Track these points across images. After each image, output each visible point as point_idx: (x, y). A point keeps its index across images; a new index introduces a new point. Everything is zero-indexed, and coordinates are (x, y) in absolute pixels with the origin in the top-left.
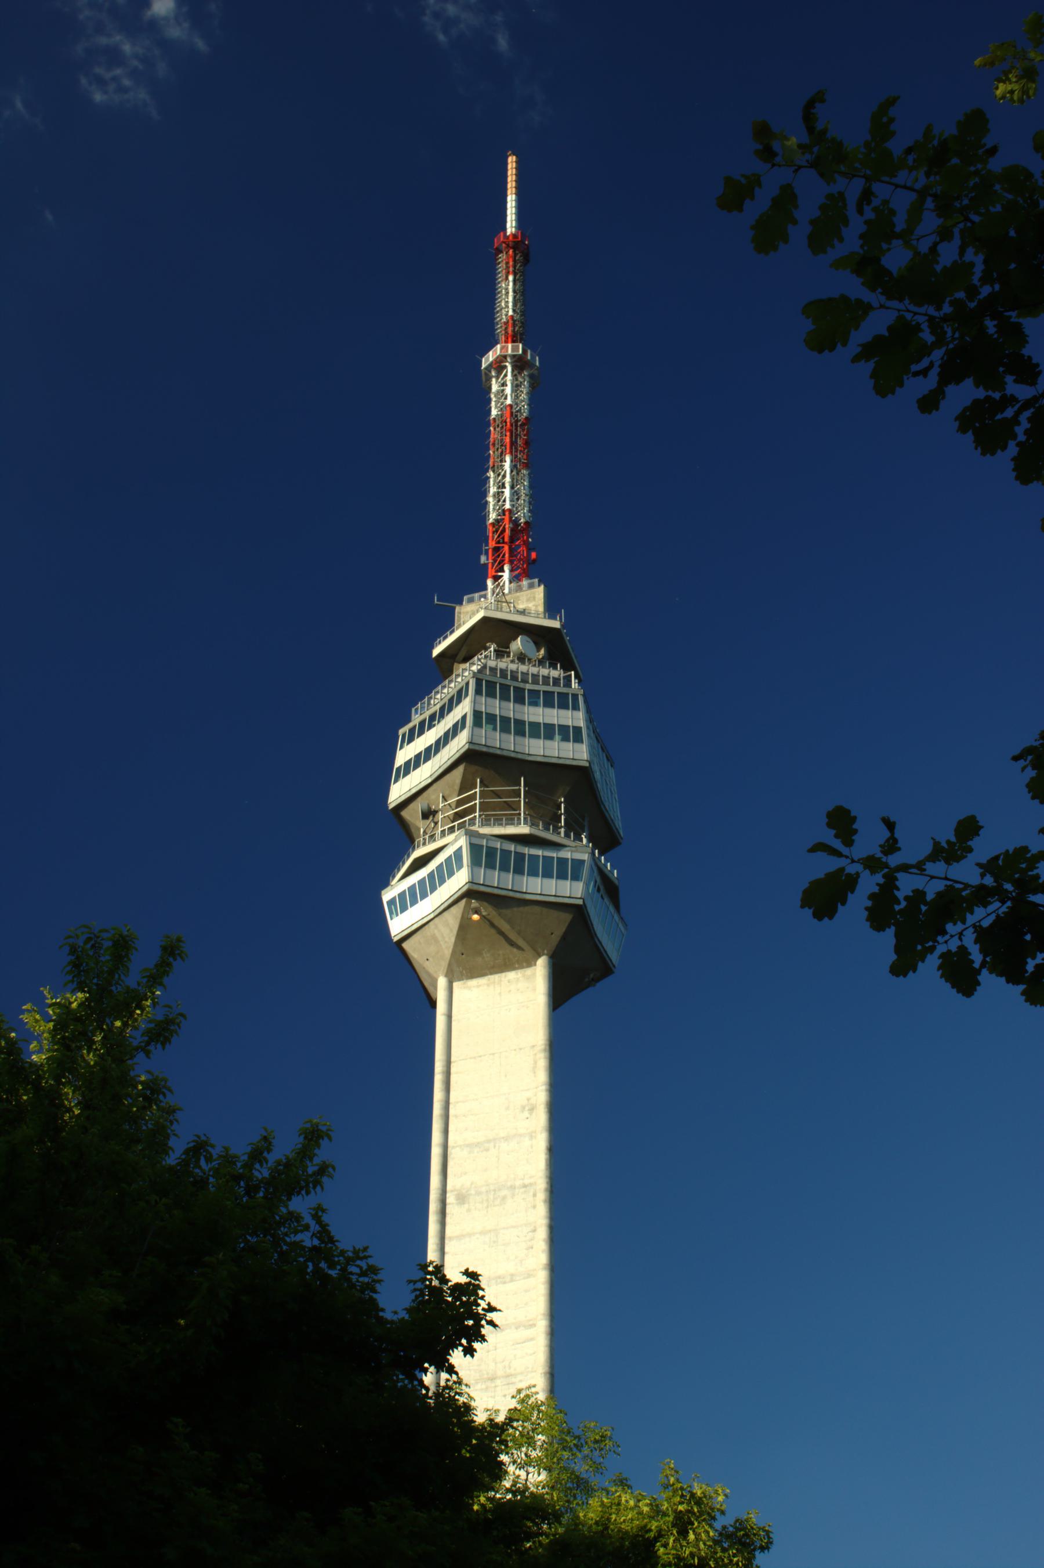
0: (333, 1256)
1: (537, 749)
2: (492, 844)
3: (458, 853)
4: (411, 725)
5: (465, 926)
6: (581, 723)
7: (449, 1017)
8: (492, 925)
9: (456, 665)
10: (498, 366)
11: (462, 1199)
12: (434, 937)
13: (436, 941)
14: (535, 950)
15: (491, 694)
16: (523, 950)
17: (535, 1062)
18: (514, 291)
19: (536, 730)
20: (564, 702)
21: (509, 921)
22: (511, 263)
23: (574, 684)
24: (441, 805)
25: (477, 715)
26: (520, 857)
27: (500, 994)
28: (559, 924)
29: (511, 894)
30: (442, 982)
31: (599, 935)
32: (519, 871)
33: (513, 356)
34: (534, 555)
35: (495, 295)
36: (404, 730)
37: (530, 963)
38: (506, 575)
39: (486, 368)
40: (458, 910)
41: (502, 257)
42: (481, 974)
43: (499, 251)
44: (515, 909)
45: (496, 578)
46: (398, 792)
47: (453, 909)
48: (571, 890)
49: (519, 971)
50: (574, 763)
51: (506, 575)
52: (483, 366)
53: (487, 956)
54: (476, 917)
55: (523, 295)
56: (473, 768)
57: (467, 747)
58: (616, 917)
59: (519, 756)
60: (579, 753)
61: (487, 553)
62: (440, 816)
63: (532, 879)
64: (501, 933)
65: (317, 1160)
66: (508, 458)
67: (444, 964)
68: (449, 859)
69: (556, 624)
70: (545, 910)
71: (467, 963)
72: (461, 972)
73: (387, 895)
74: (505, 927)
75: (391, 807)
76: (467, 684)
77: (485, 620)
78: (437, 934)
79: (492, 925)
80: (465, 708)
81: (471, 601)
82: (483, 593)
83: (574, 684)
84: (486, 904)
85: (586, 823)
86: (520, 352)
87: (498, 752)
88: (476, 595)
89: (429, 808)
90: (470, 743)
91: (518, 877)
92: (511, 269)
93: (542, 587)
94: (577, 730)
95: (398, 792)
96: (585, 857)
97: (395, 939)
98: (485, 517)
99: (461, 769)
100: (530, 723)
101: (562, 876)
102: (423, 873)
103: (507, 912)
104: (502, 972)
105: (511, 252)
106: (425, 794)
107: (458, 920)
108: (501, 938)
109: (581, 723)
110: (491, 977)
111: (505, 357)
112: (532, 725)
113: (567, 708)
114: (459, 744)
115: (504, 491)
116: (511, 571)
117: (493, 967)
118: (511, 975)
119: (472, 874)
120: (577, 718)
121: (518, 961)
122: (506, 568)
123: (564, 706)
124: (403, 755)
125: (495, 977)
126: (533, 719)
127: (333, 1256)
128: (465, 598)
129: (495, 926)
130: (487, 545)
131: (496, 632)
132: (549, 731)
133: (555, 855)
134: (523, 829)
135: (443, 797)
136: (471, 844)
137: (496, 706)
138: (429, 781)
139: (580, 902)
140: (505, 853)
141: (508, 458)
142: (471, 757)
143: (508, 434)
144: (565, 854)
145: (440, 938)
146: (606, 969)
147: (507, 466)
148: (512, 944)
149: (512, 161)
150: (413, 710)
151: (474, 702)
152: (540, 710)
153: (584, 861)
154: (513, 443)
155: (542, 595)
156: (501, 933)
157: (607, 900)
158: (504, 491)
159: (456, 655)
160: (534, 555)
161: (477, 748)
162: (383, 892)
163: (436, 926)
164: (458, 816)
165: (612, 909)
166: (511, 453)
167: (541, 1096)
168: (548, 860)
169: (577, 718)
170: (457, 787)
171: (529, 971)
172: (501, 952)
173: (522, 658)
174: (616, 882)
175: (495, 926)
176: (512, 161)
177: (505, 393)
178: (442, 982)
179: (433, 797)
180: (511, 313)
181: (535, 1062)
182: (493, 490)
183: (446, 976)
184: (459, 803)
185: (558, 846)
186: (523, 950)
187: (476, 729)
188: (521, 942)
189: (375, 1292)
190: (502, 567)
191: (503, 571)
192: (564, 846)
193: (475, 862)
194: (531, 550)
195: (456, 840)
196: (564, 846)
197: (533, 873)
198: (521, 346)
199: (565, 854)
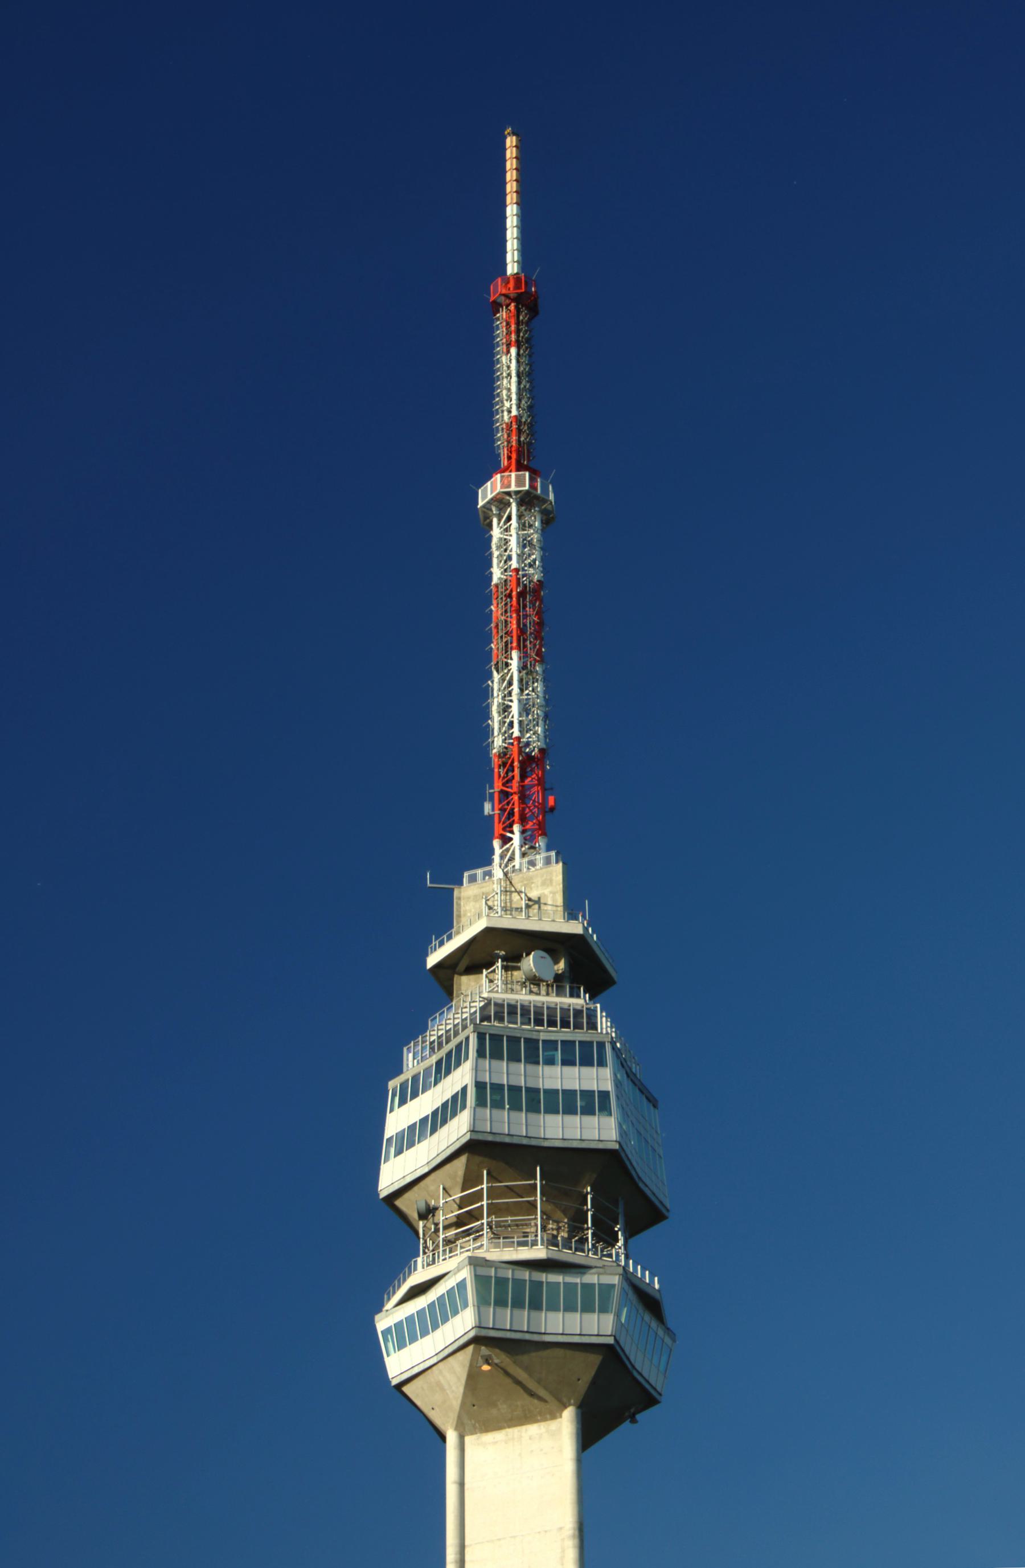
1: (558, 1129)
2: (502, 1273)
3: (462, 1285)
4: (402, 1078)
5: (473, 1377)
6: (608, 1086)
7: (461, 1484)
8: (507, 1373)
9: (456, 977)
10: (501, 502)
12: (439, 1384)
13: (442, 1389)
14: (560, 1401)
16: (545, 1401)
17: (563, 1551)
18: (518, 375)
19: (535, 1101)
20: (587, 1055)
21: (527, 1369)
22: (513, 327)
23: (604, 1024)
24: (442, 1202)
25: (480, 1086)
26: (537, 1286)
27: (520, 1455)
28: (587, 1368)
29: (527, 1337)
31: (638, 1366)
32: (536, 1305)
33: (517, 493)
34: (551, 801)
35: (493, 389)
36: (394, 1084)
37: (554, 1415)
38: (516, 838)
39: (484, 506)
40: (460, 1364)
41: (503, 314)
42: (499, 1428)
43: (496, 306)
44: (533, 1354)
45: (506, 840)
46: (393, 1173)
47: (460, 1355)
48: (598, 1326)
49: (543, 1424)
50: (601, 1146)
51: (516, 838)
52: (481, 503)
53: (504, 1408)
54: (486, 1368)
55: (528, 376)
56: (478, 1159)
57: (468, 1137)
58: (661, 1332)
59: (534, 1142)
60: (601, 1131)
61: (492, 799)
62: (441, 1218)
63: (551, 1315)
64: (519, 1383)
66: (515, 654)
67: (453, 1416)
68: (450, 1292)
69: (575, 928)
70: (569, 1353)
71: (483, 1411)
72: (474, 1426)
73: (383, 1322)
74: (522, 1375)
75: (383, 1194)
76: (467, 1039)
78: (443, 1381)
79: (507, 1373)
80: (462, 1077)
81: (473, 879)
82: (487, 869)
83: (604, 1024)
84: (497, 1351)
86: (527, 487)
87: (507, 1140)
88: (479, 872)
89: (427, 1205)
90: (473, 1131)
91: (534, 1314)
92: (513, 337)
93: (561, 864)
94: (604, 1095)
95: (393, 1173)
96: (615, 1280)
97: (394, 1382)
98: (489, 746)
99: (463, 1160)
100: (546, 1091)
101: (587, 1308)
103: (525, 1358)
104: (522, 1424)
105: (512, 307)
106: (422, 1184)
107: (466, 1369)
108: (519, 1388)
109: (608, 1086)
110: (510, 1431)
111: (509, 494)
112: (552, 1093)
113: (591, 1065)
114: (457, 1130)
115: (512, 707)
116: (523, 832)
117: (511, 1420)
118: (533, 1429)
119: (479, 1315)
121: (540, 1413)
122: (516, 828)
124: (398, 1120)
125: (514, 1432)
126: (550, 1084)
128: (466, 874)
129: (510, 1370)
130: (491, 787)
132: (570, 1102)
133: (578, 1280)
134: (539, 1252)
135: (444, 1189)
136: (476, 1275)
137: (505, 1072)
138: (426, 1170)
139: (611, 1341)
140: (519, 1283)
141: (515, 654)
142: (475, 1148)
143: (514, 615)
144: (591, 1278)
145: (446, 1387)
146: (649, 1399)
147: (514, 664)
148: (532, 1394)
149: (511, 141)
150: (405, 1049)
151: (476, 1069)
152: (557, 1070)
153: (613, 1286)
154: (522, 631)
155: (560, 878)
156: (519, 1383)
157: (647, 1317)
158: (512, 707)
159: (456, 965)
160: (551, 801)
161: (480, 1137)
162: (377, 1317)
163: (441, 1372)
164: (459, 1222)
165: (654, 1324)
166: (519, 648)
168: (570, 1288)
169: (599, 1078)
170: (460, 1180)
171: (553, 1425)
172: (519, 1403)
173: (534, 981)
174: (657, 1296)
175: (510, 1370)
176: (511, 141)
177: (510, 548)
178: (452, 1437)
179: (432, 1188)
180: (514, 412)
181: (563, 1551)
183: (456, 1429)
184: (462, 1203)
185: (580, 1268)
186: (545, 1401)
187: (479, 1110)
188: (542, 1392)
190: (511, 825)
191: (512, 832)
192: (590, 1267)
193: (482, 1301)
194: (546, 800)
195: (459, 1269)
196: (590, 1267)
197: (553, 1307)
198: (527, 474)
199: (591, 1278)
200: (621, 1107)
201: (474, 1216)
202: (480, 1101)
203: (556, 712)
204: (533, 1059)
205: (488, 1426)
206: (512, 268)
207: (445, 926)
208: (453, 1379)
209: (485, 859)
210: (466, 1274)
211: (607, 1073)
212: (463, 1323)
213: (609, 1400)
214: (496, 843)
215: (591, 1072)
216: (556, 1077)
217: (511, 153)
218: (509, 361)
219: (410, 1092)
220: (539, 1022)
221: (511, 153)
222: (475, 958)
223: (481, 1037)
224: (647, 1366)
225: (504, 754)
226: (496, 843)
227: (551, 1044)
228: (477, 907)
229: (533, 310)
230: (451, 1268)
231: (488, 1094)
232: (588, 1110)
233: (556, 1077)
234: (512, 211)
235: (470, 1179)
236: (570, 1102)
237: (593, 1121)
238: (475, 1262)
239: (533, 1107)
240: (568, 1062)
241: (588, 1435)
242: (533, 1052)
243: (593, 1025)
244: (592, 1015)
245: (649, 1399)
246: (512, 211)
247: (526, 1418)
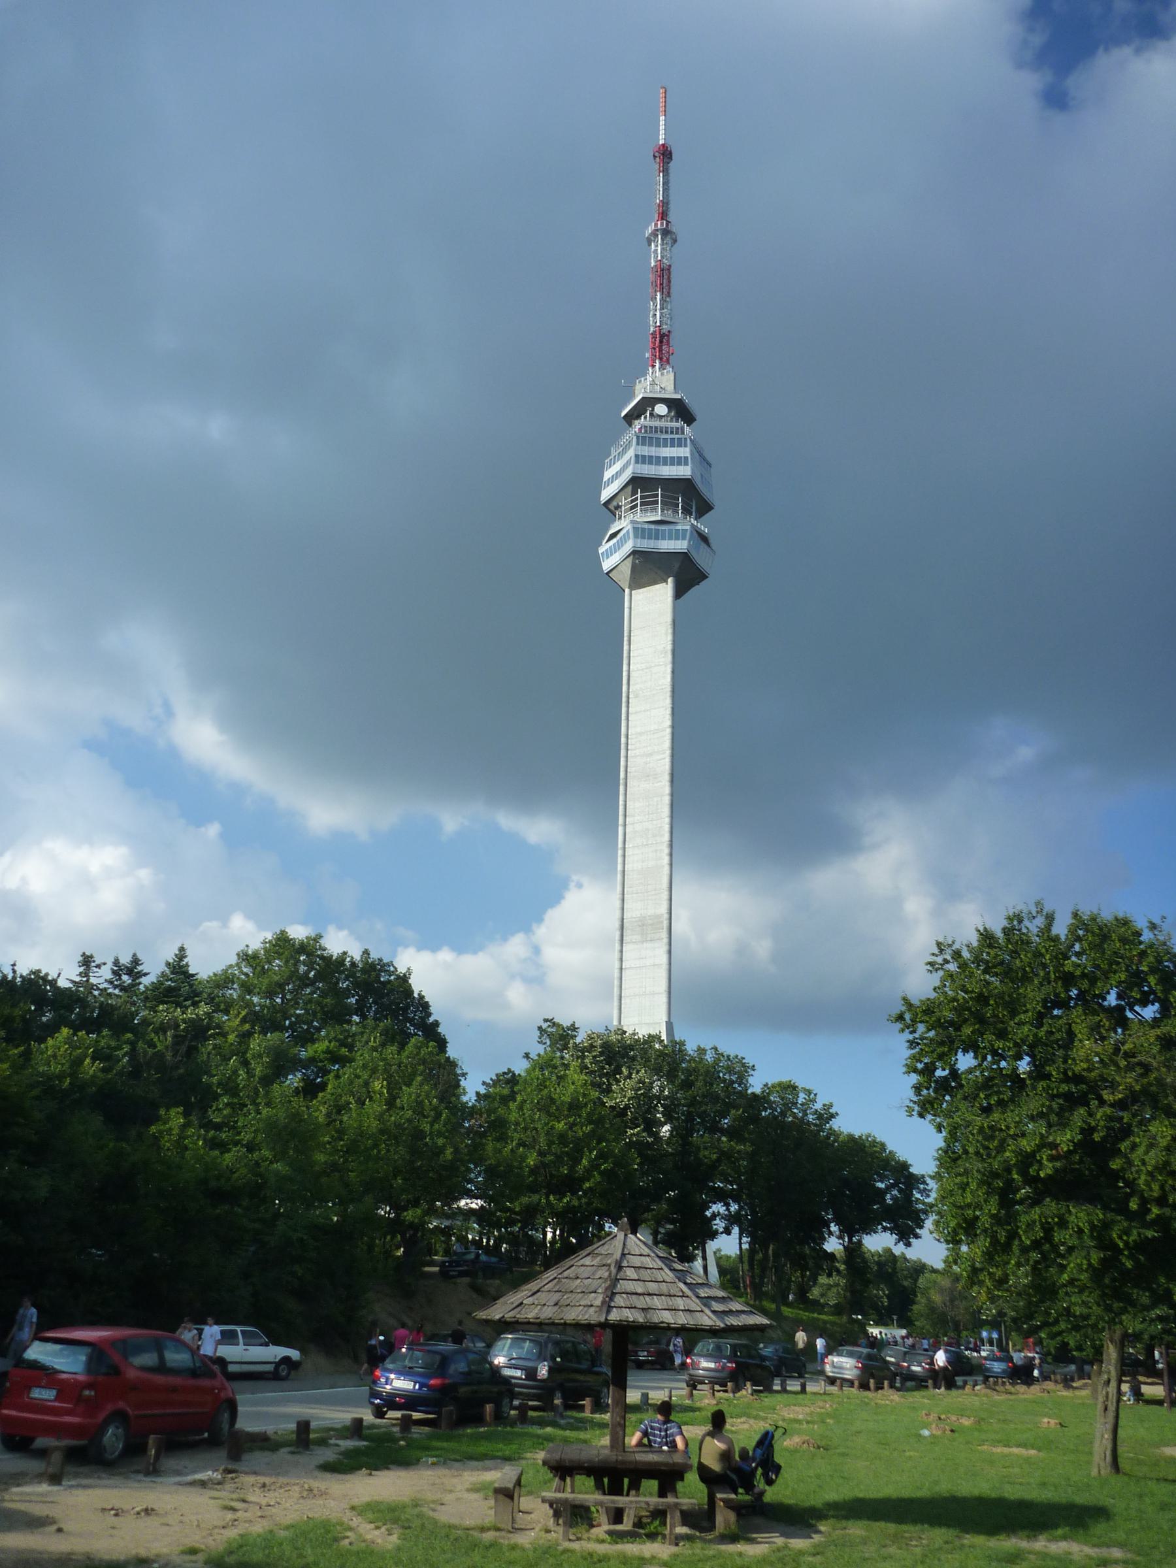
1: (667, 471)
6: (688, 455)
7: (630, 608)
11: (637, 696)
19: (666, 461)
20: (680, 443)
25: (637, 456)
30: (627, 591)
32: (657, 538)
38: (657, 365)
40: (630, 559)
45: (653, 366)
48: (681, 545)
51: (657, 365)
60: (684, 471)
69: (678, 396)
73: (601, 550)
77: (643, 398)
80: (631, 453)
85: (694, 510)
94: (686, 458)
96: (688, 527)
102: (614, 541)
109: (688, 455)
123: (680, 445)
124: (608, 475)
132: (672, 461)
134: (659, 518)
137: (646, 451)
144: (679, 527)
147: (658, 297)
167: (669, 647)
169: (685, 452)
175: (647, 566)
178: (627, 591)
193: (636, 537)
197: (664, 538)
199: (679, 527)
200: (693, 462)
204: (658, 445)
208: (627, 568)
210: (630, 527)
211: (688, 449)
212: (628, 547)
213: (686, 574)
215: (682, 449)
216: (668, 452)
217: (662, 123)
221: (662, 123)
224: (702, 559)
230: (623, 524)
231: (640, 459)
232: (679, 464)
233: (668, 452)
235: (634, 493)
236: (672, 461)
237: (681, 468)
238: (632, 522)
239: (658, 463)
240: (672, 446)
241: (679, 593)
242: (659, 443)
244: (682, 429)
245: (703, 576)
247: (655, 582)
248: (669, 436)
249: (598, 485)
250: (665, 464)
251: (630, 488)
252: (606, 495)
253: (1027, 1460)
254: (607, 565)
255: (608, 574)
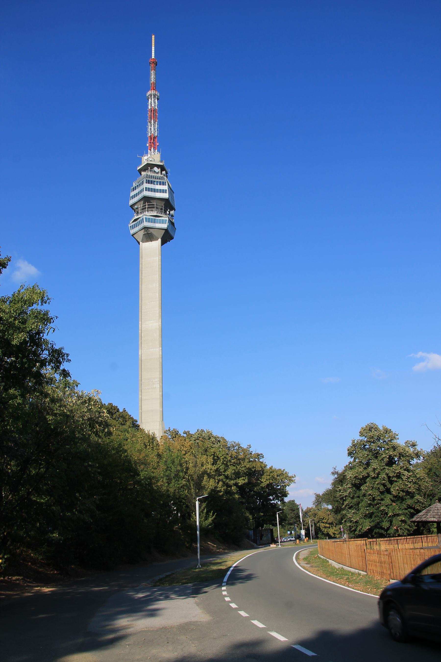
0: (48, 421)
10: (151, 95)
15: (149, 183)
19: (155, 190)
20: (164, 184)
45: (150, 150)
48: (165, 226)
55: (156, 74)
60: (166, 196)
65: (361, 438)
69: (162, 164)
94: (166, 190)
96: (167, 219)
101: (163, 223)
115: (153, 129)
120: (166, 187)
122: (152, 148)
123: (163, 185)
127: (48, 421)
131: (149, 166)
147: (152, 122)
149: (153, 36)
158: (153, 129)
164: (142, 209)
169: (166, 187)
171: (157, 241)
176: (153, 36)
182: (149, 127)
189: (126, 451)
201: (145, 208)
202: (146, 190)
203: (160, 129)
205: (147, 241)
206: (153, 57)
207: (140, 163)
209: (147, 153)
213: (167, 237)
214: (149, 151)
215: (164, 186)
218: (153, 72)
219: (134, 189)
220: (156, 178)
222: (145, 168)
223: (146, 180)
225: (151, 136)
226: (149, 151)
227: (157, 182)
228: (145, 160)
229: (156, 65)
234: (153, 48)
241: (163, 243)
242: (152, 182)
243: (164, 179)
245: (172, 238)
246: (153, 48)
248: (159, 180)
249: (129, 198)
250: (158, 192)
251: (142, 202)
252: (132, 202)
253: (196, 522)
254: (132, 232)
255: (133, 235)
